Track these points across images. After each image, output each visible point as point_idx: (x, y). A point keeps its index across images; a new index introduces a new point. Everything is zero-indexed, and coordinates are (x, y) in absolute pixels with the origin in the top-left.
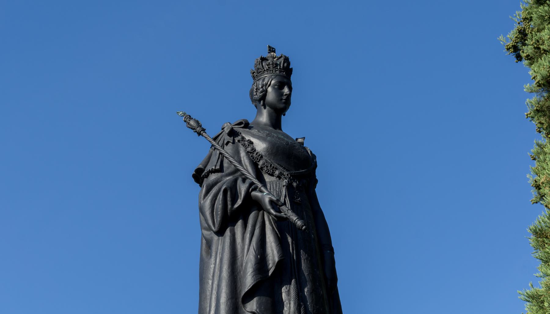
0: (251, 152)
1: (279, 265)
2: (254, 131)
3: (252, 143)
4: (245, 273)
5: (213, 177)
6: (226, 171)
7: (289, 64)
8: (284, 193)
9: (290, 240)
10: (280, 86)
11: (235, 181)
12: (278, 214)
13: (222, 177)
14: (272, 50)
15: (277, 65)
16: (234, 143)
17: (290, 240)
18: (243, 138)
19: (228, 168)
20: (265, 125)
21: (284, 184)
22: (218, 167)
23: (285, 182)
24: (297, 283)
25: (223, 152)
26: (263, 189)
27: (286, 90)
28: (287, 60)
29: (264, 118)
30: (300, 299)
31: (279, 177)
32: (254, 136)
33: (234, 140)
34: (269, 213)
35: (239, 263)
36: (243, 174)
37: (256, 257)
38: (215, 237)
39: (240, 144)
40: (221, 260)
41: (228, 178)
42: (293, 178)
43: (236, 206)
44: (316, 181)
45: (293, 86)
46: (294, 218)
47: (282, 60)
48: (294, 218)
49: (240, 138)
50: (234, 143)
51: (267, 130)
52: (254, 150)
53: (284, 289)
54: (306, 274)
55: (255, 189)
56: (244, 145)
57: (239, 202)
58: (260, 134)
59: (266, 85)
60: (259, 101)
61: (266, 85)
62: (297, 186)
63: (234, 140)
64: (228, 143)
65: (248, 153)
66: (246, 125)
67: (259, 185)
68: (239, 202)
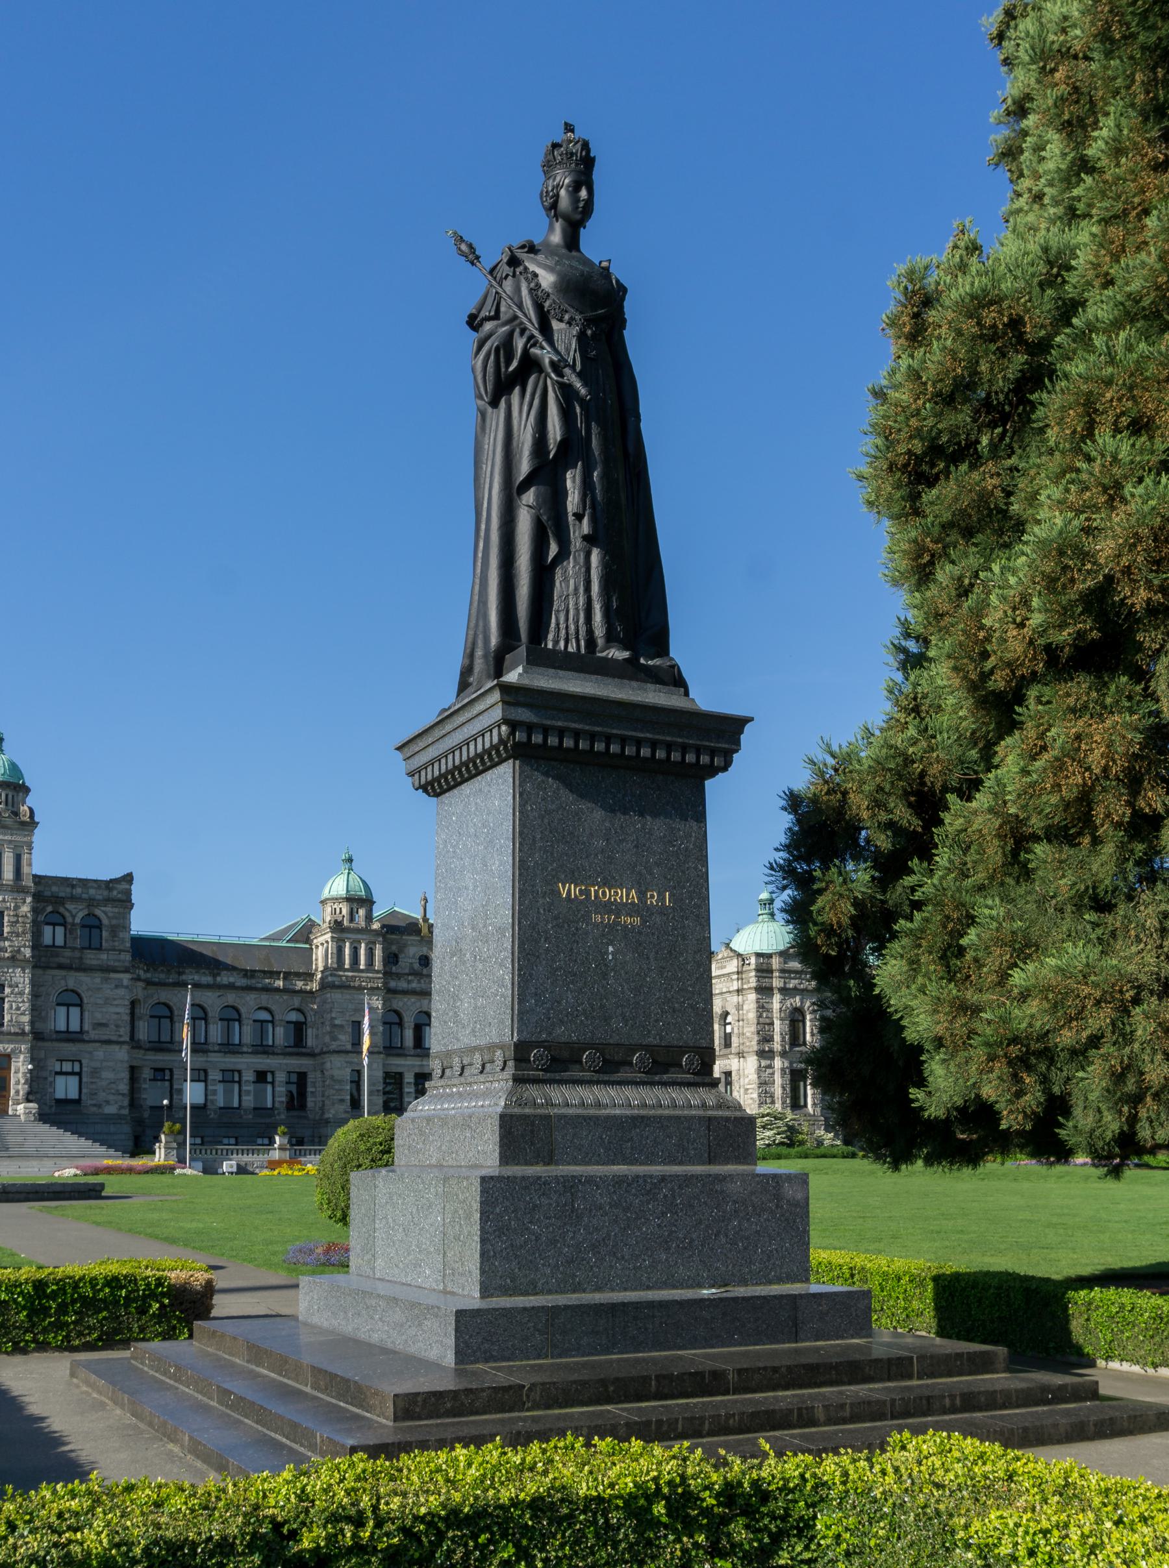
0: (535, 290)
1: (563, 445)
2: (540, 257)
3: (536, 275)
4: (521, 458)
5: (488, 326)
6: (504, 317)
7: (588, 151)
8: (573, 346)
9: (578, 410)
10: (576, 187)
11: (511, 334)
12: (560, 379)
13: (497, 327)
14: (569, 128)
15: (572, 154)
16: (514, 276)
17: (578, 410)
18: (526, 268)
19: (506, 313)
20: (557, 246)
21: (575, 333)
22: (492, 313)
23: (575, 330)
24: (583, 466)
25: (500, 290)
26: (544, 344)
27: (583, 193)
28: (586, 145)
29: (556, 238)
30: (587, 485)
31: (569, 323)
32: (540, 265)
33: (514, 273)
34: (551, 378)
35: (515, 444)
36: (522, 323)
37: (534, 437)
38: (490, 410)
39: (522, 278)
40: (495, 439)
41: (504, 329)
42: (588, 322)
43: (511, 369)
44: (624, 321)
45: (595, 187)
46: (578, 384)
47: (579, 146)
48: (578, 384)
49: (521, 268)
50: (514, 276)
51: (556, 255)
52: (538, 285)
53: (569, 475)
54: (597, 453)
55: (534, 345)
56: (527, 279)
57: (515, 364)
58: (548, 263)
59: (558, 187)
60: (550, 209)
61: (558, 187)
62: (594, 334)
63: (514, 273)
64: (507, 276)
65: (531, 290)
66: (532, 249)
67: (540, 338)
68: (515, 364)
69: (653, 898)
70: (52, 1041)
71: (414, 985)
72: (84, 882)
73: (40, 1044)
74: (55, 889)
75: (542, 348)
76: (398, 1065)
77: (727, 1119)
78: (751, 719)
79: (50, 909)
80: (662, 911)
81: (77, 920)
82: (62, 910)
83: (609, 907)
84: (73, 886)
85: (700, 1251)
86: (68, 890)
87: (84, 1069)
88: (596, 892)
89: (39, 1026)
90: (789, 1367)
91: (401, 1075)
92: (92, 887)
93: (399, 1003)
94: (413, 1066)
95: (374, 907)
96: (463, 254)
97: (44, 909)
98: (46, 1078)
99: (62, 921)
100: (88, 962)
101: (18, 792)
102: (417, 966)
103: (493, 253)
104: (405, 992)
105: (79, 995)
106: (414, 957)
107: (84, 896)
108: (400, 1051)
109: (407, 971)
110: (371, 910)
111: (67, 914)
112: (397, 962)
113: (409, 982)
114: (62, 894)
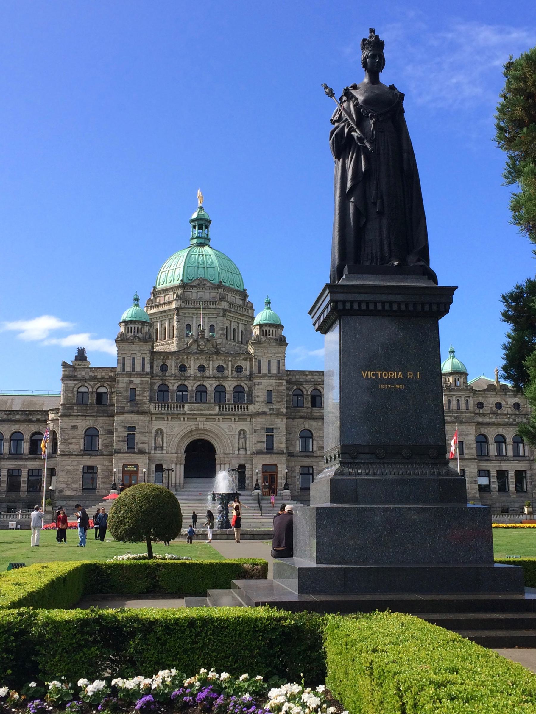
11: (343, 128)
52: (357, 103)
65: (354, 106)
69: (410, 375)
70: (298, 456)
71: (493, 420)
72: (312, 373)
73: (292, 458)
74: (297, 377)
75: (356, 132)
76: (486, 466)
77: (450, 480)
78: (457, 287)
79: (295, 387)
80: (416, 381)
81: (309, 393)
82: (301, 388)
83: (390, 381)
84: (306, 375)
85: (430, 545)
86: (304, 377)
87: (314, 471)
88: (381, 375)
89: (291, 449)
90: (457, 600)
91: (489, 471)
92: (316, 375)
93: (484, 430)
94: (495, 466)
95: (468, 377)
96: (327, 93)
97: (292, 387)
98: (295, 477)
99: (301, 394)
100: (315, 414)
101: (278, 329)
102: (494, 409)
103: (339, 92)
104: (488, 424)
105: (311, 432)
106: (492, 404)
107: (312, 380)
108: (487, 458)
109: (489, 412)
110: (466, 379)
111: (304, 390)
112: (483, 407)
113: (490, 418)
114: (301, 380)
